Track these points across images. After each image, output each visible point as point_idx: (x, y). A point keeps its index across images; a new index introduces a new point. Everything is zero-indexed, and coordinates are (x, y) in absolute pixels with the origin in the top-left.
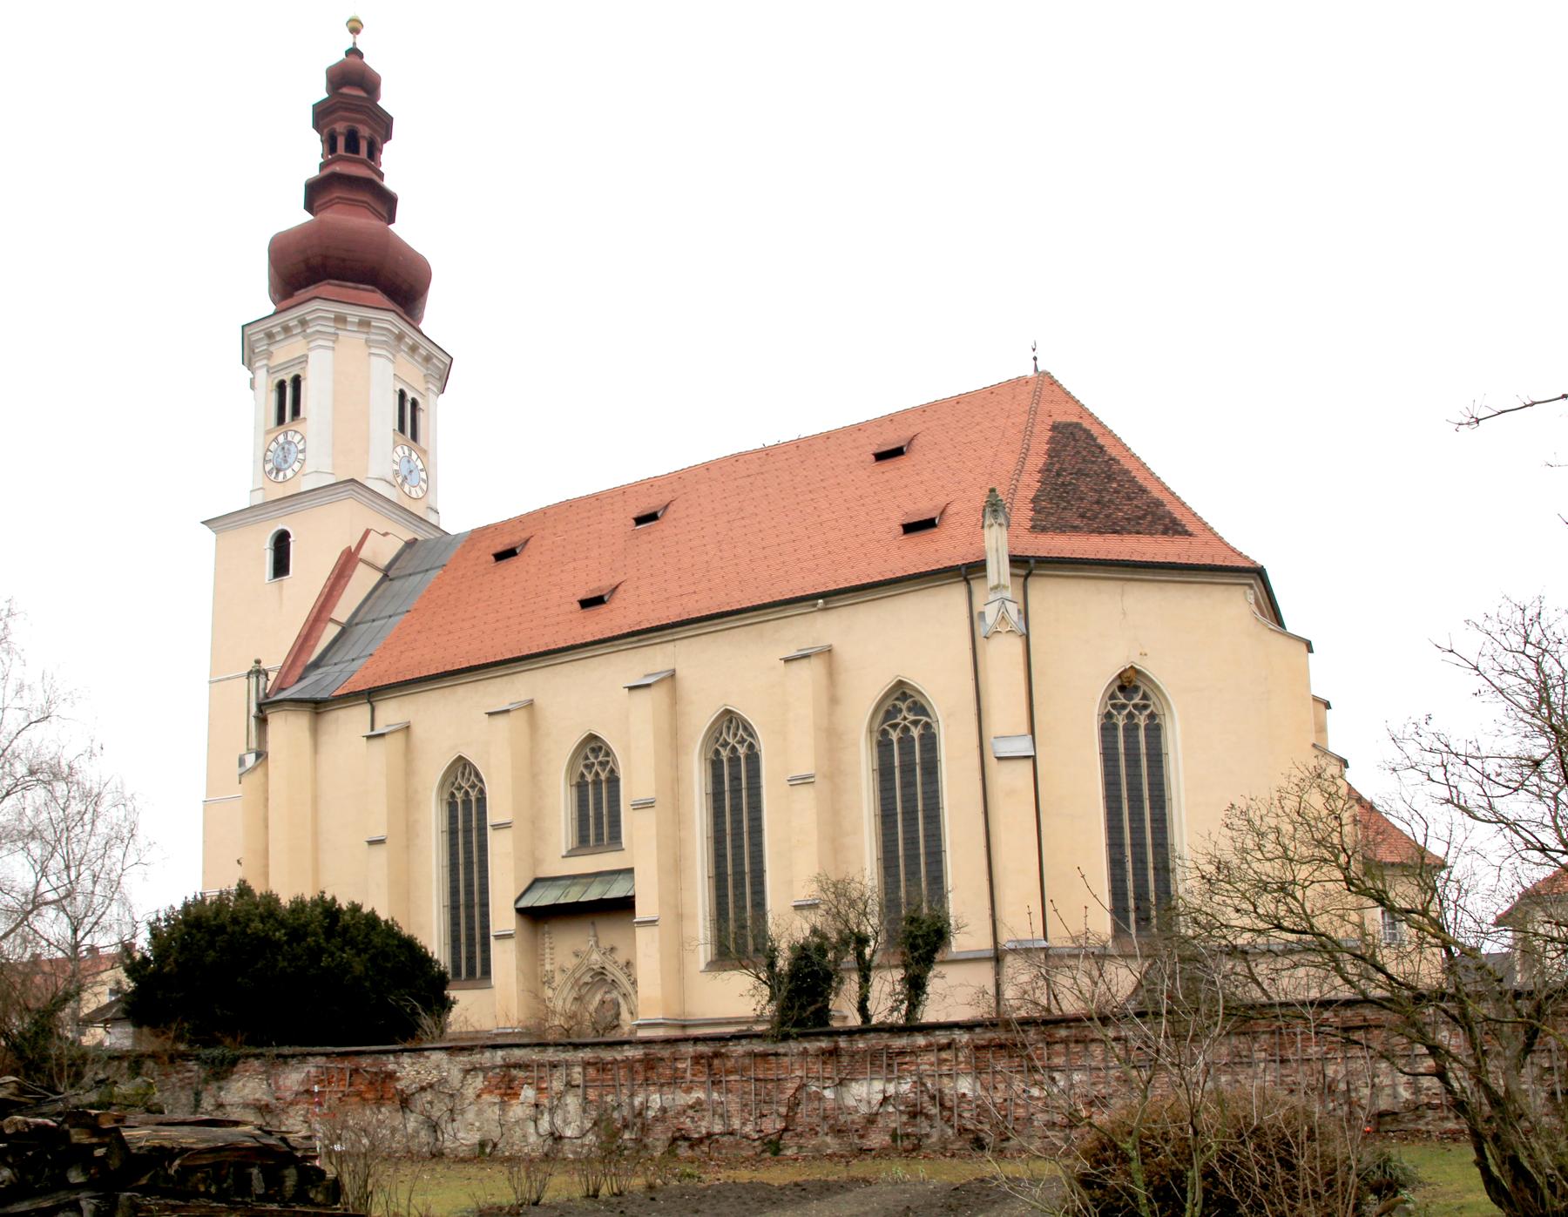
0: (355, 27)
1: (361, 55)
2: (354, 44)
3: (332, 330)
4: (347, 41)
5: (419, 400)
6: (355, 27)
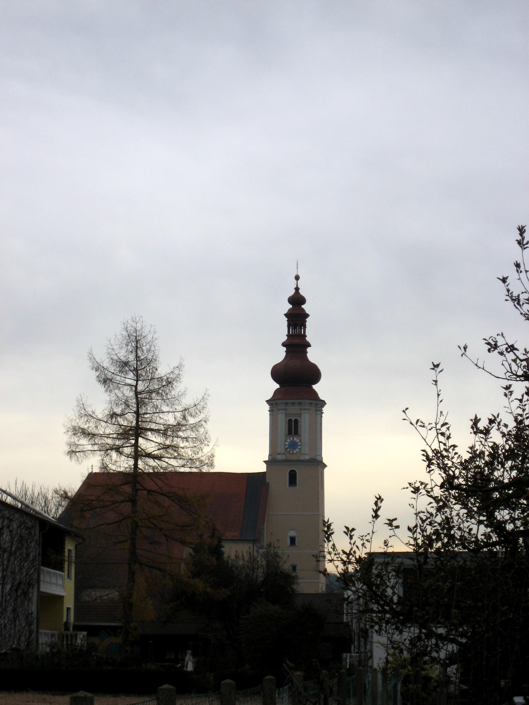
0: (297, 278)
1: (302, 300)
2: (297, 289)
3: (284, 407)
4: (293, 284)
5: (298, 419)
6: (297, 278)
